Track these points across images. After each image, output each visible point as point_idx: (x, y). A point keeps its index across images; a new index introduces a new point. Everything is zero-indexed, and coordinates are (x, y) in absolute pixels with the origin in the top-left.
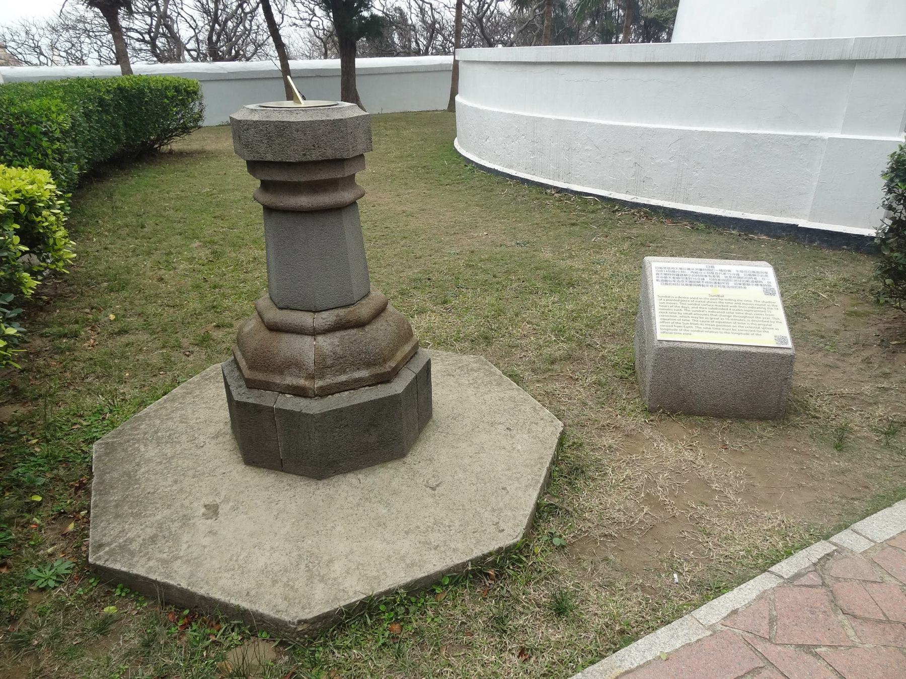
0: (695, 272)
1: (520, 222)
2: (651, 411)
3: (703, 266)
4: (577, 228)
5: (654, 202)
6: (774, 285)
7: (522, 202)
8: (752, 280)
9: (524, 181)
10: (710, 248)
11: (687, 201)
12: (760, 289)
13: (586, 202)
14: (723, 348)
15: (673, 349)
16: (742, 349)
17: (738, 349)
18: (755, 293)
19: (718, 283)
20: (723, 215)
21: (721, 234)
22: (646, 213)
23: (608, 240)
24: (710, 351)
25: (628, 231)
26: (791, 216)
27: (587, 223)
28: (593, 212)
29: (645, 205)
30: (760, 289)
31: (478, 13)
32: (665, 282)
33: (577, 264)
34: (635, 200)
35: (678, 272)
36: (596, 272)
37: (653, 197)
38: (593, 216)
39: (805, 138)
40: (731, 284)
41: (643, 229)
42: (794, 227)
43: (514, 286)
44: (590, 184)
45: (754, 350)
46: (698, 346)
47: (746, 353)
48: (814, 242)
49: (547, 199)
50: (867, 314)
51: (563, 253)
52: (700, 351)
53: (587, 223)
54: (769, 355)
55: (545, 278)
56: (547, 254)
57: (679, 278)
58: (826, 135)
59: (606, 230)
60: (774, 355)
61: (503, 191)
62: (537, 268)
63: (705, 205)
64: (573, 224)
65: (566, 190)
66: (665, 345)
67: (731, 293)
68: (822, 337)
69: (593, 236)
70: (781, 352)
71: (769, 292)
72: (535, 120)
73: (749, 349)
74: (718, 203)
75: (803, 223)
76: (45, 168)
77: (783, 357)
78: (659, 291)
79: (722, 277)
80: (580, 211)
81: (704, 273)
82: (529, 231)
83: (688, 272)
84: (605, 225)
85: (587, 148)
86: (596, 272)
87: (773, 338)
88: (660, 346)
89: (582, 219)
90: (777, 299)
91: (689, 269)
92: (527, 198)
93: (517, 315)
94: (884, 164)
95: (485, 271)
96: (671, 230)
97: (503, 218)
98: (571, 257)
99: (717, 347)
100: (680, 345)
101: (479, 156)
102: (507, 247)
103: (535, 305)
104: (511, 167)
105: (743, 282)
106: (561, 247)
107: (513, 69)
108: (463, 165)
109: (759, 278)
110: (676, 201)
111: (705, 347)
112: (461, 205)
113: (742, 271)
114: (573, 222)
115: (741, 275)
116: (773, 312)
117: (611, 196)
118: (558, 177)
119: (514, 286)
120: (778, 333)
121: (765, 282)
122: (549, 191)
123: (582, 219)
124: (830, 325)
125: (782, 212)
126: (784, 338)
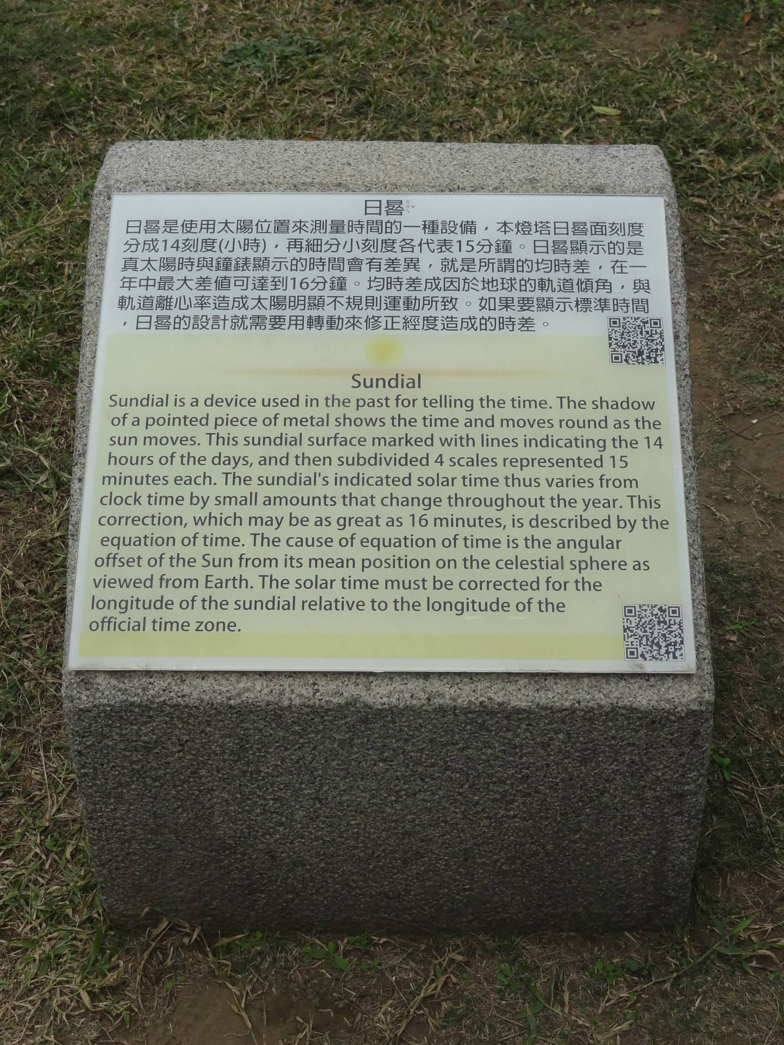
0: (308, 240)
2: (120, 930)
3: (346, 206)
6: (662, 303)
12: (592, 327)
15: (147, 711)
16: (466, 695)
17: (448, 694)
18: (567, 352)
19: (407, 305)
30: (592, 327)
32: (160, 312)
35: (230, 244)
40: (468, 304)
45: (520, 697)
52: (275, 714)
54: (591, 716)
60: (613, 713)
66: (108, 694)
67: (453, 359)
70: (644, 698)
71: (631, 345)
73: (497, 694)
76: (718, 693)
78: (128, 359)
79: (430, 264)
81: (350, 245)
83: (276, 246)
87: (617, 622)
88: (85, 699)
90: (661, 386)
91: (281, 226)
99: (350, 691)
109: (599, 265)
111: (297, 695)
113: (524, 227)
116: (642, 462)
126: (666, 615)
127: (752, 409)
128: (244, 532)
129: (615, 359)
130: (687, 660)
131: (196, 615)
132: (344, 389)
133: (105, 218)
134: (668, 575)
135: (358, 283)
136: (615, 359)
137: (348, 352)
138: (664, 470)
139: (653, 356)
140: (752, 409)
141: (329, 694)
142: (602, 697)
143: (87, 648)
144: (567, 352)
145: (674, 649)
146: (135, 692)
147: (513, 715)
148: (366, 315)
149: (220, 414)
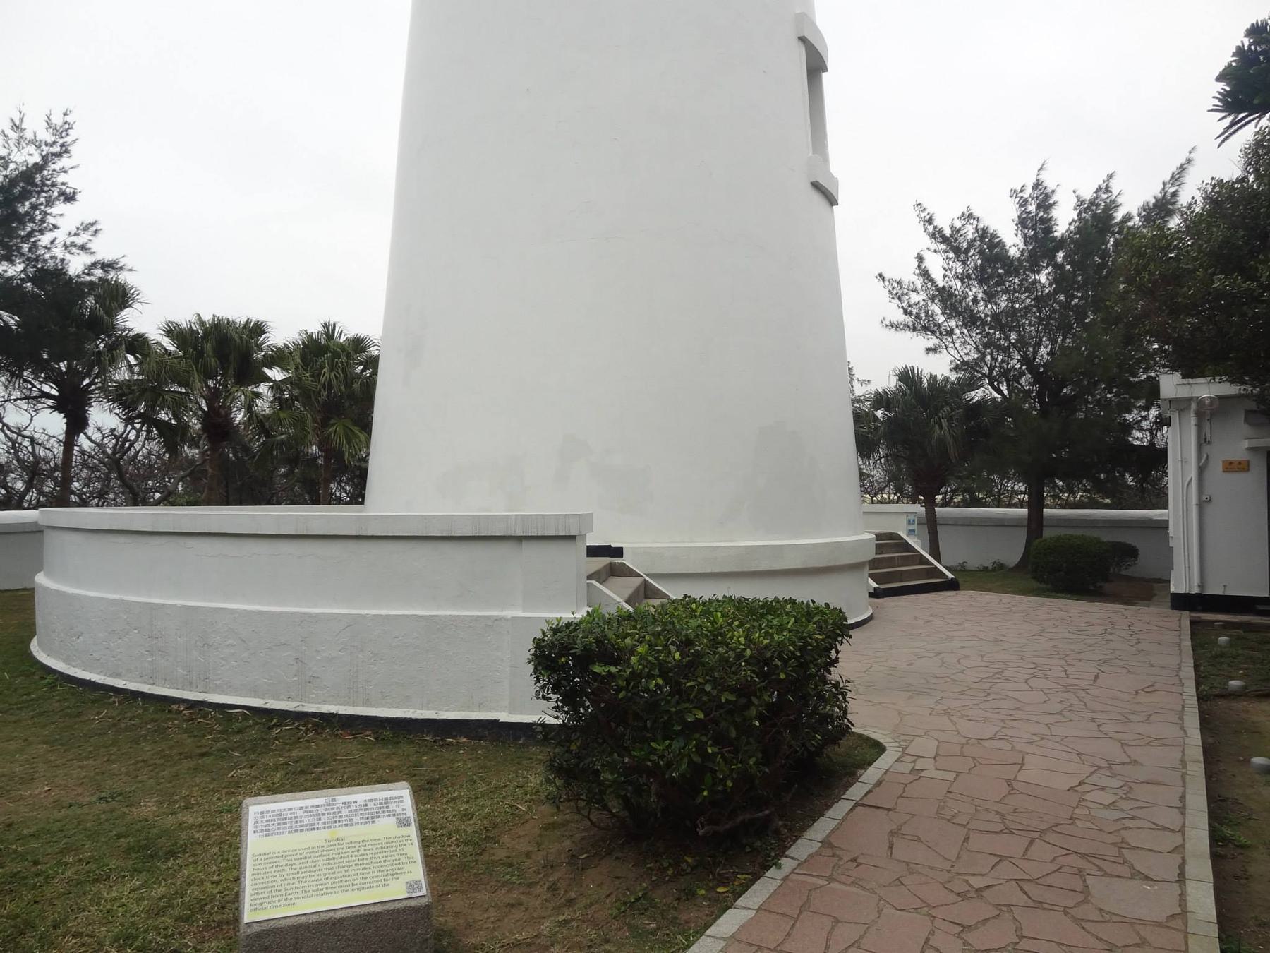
0: (308, 811)
1: (114, 762)
4: (208, 760)
5: (325, 709)
7: (127, 729)
8: (384, 809)
9: (136, 695)
10: (395, 763)
11: (367, 703)
12: (393, 820)
13: (230, 719)
14: (338, 915)
16: (364, 911)
17: (358, 911)
18: (386, 827)
19: (339, 822)
20: (414, 716)
21: (413, 742)
22: (315, 724)
23: (253, 772)
24: (320, 923)
25: (287, 754)
26: (491, 710)
27: (225, 751)
28: (240, 731)
29: (314, 715)
30: (393, 820)
31: (114, 453)
33: (188, 818)
34: (300, 709)
35: (287, 814)
36: (220, 826)
37: (324, 702)
38: (237, 738)
39: (488, 617)
41: (307, 748)
42: (495, 723)
43: (67, 874)
44: (236, 692)
45: (378, 909)
46: (303, 920)
47: (369, 914)
48: (519, 738)
49: (169, 719)
50: (565, 824)
51: (175, 802)
52: (308, 927)
53: (225, 751)
55: (129, 850)
56: (149, 808)
57: (285, 824)
58: (509, 613)
59: (253, 757)
61: (98, 714)
62: (119, 836)
63: (391, 706)
64: (203, 755)
65: (203, 703)
66: (257, 928)
68: (511, 865)
69: (232, 768)
70: (413, 903)
71: (403, 823)
72: (152, 607)
73: (372, 909)
74: (406, 702)
75: (504, 717)
77: (416, 910)
78: (255, 845)
79: (345, 812)
80: (220, 732)
82: (127, 774)
83: (300, 813)
84: (253, 750)
85: (230, 642)
86: (220, 826)
88: (249, 932)
89: (219, 745)
90: (412, 832)
92: (137, 721)
93: (55, 927)
94: (527, 650)
95: (22, 856)
96: (350, 747)
97: (87, 758)
98: (188, 807)
99: (330, 915)
100: (277, 924)
101: (67, 661)
102: (81, 806)
103: (97, 900)
104: (117, 675)
105: (371, 816)
106: (174, 794)
107: (121, 539)
108: (37, 677)
109: (392, 806)
110: (354, 704)
111: (313, 919)
112: (13, 746)
114: (205, 750)
115: (370, 805)
117: (267, 706)
118: (190, 686)
119: (67, 874)
120: (410, 878)
121: (399, 811)
122: (175, 707)
123: (219, 745)
124: (523, 846)
125: (480, 706)
126: (417, 882)
127: (449, 893)
128: (296, 881)
129: (362, 503)
130: (424, 892)
131: (284, 902)
132: (323, 843)
133: (247, 813)
134: (417, 872)
135: (325, 819)
136: (362, 503)
137: (325, 834)
138: (415, 851)
139: (409, 825)
140: (449, 893)
141: (323, 917)
142: (402, 905)
143: (249, 915)
144: (386, 827)
145: (420, 890)
146: (265, 926)
147: (377, 915)
148: (328, 825)
149: (287, 854)
